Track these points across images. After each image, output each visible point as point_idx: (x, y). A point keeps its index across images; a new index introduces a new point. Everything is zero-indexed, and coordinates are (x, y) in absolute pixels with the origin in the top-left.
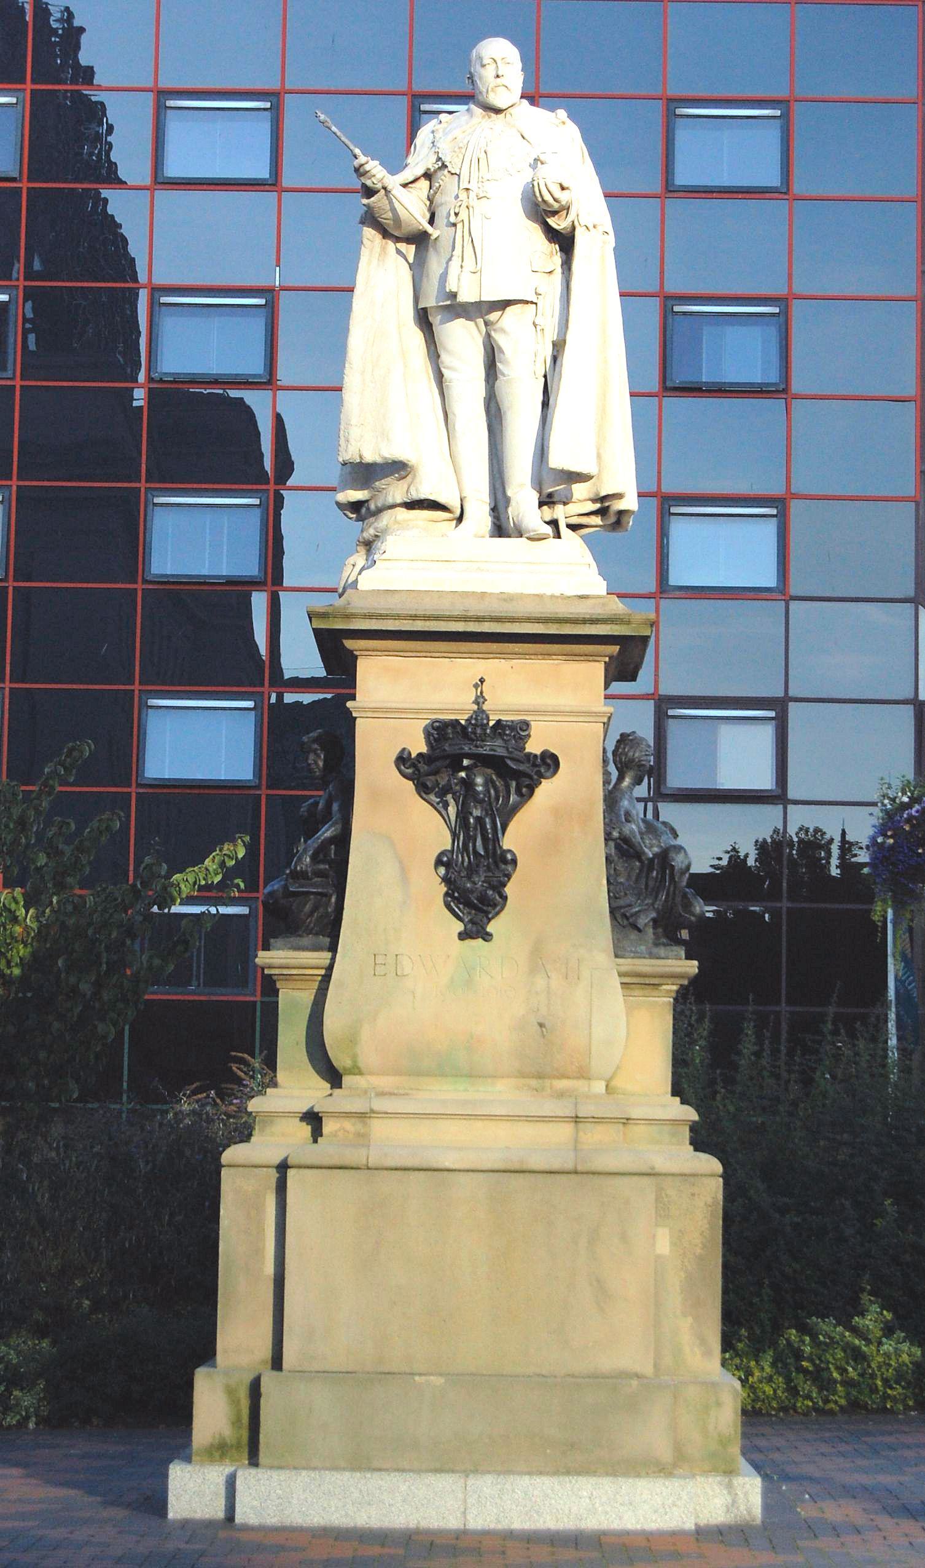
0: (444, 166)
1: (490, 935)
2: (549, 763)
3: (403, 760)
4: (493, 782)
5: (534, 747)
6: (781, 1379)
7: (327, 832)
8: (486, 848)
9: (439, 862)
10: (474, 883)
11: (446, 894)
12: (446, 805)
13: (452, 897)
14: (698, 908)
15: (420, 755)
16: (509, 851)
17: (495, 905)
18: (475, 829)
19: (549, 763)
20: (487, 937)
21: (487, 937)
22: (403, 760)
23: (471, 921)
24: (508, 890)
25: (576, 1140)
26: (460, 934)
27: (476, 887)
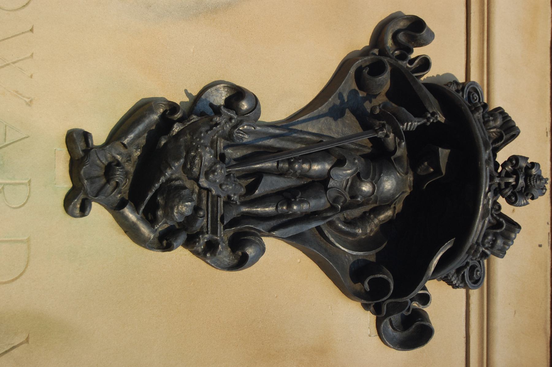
1: (84, 210)
4: (376, 211)
6: (412, 179)
9: (237, 94)
10: (211, 171)
11: (173, 107)
12: (336, 113)
13: (166, 123)
14: (510, 167)
16: (262, 250)
17: (150, 218)
18: (304, 175)
20: (77, 202)
21: (77, 202)
23: (109, 170)
24: (180, 255)
26: (86, 136)
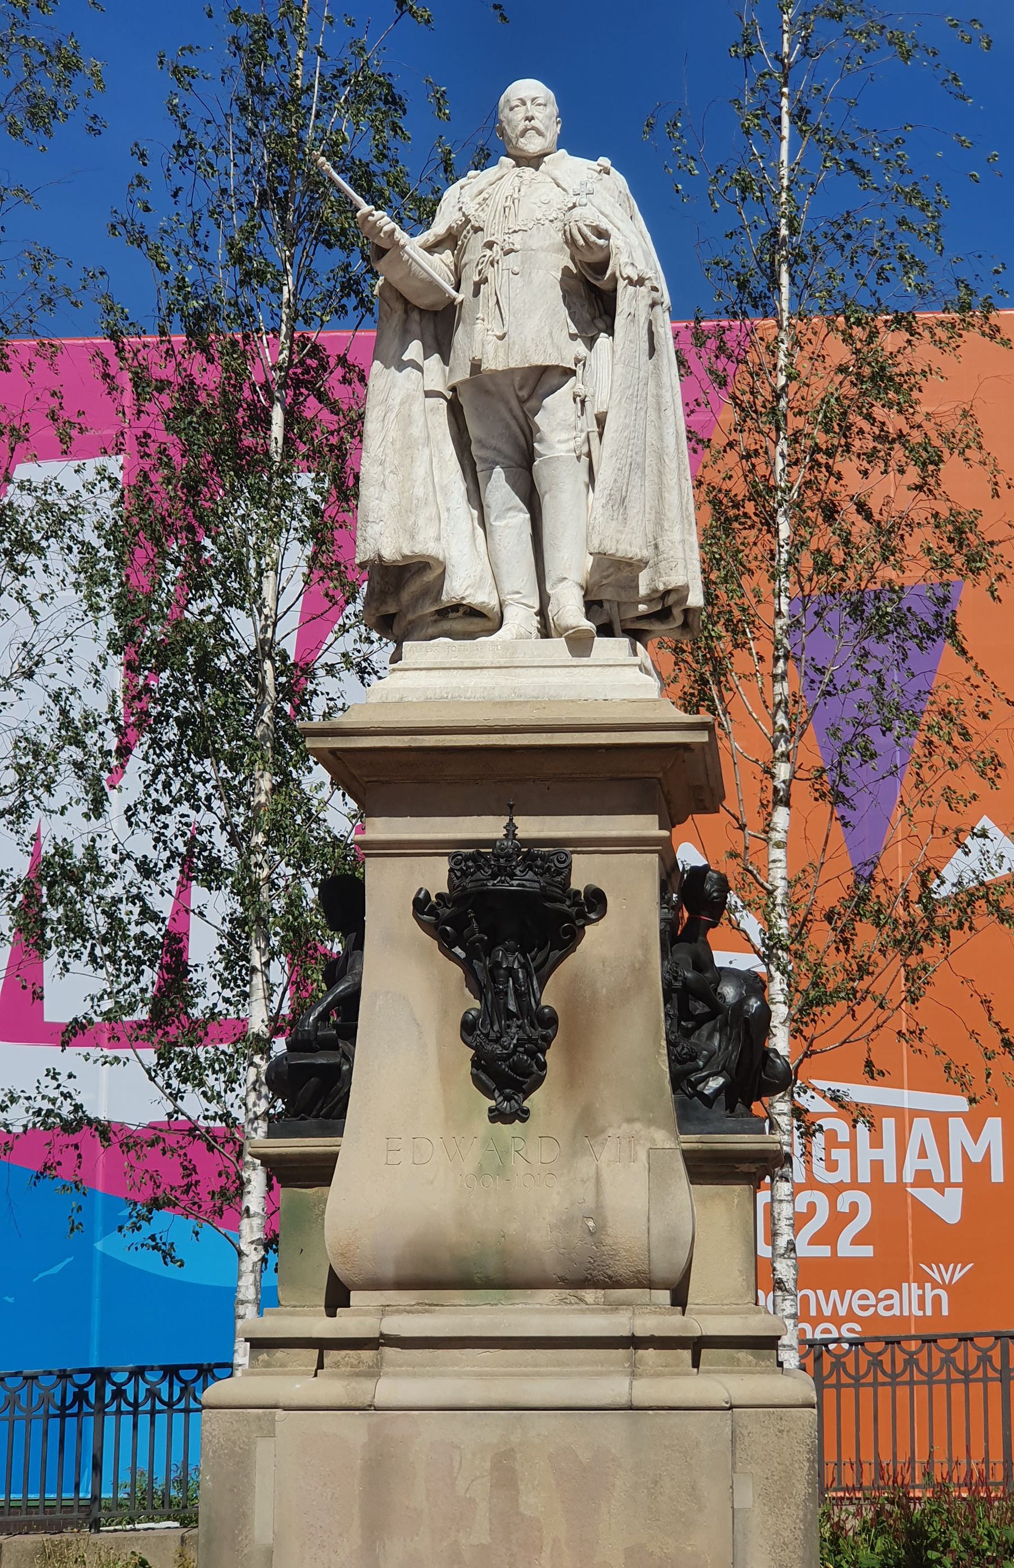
0: (468, 221)
2: (595, 902)
3: (421, 905)
5: (578, 883)
7: (909, 1201)
8: (519, 1006)
15: (439, 896)
19: (595, 902)
20: (523, 1115)
22: (421, 905)
25: (247, 1302)
27: (507, 1061)
